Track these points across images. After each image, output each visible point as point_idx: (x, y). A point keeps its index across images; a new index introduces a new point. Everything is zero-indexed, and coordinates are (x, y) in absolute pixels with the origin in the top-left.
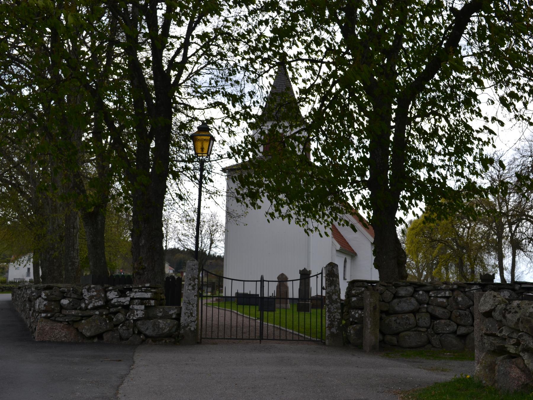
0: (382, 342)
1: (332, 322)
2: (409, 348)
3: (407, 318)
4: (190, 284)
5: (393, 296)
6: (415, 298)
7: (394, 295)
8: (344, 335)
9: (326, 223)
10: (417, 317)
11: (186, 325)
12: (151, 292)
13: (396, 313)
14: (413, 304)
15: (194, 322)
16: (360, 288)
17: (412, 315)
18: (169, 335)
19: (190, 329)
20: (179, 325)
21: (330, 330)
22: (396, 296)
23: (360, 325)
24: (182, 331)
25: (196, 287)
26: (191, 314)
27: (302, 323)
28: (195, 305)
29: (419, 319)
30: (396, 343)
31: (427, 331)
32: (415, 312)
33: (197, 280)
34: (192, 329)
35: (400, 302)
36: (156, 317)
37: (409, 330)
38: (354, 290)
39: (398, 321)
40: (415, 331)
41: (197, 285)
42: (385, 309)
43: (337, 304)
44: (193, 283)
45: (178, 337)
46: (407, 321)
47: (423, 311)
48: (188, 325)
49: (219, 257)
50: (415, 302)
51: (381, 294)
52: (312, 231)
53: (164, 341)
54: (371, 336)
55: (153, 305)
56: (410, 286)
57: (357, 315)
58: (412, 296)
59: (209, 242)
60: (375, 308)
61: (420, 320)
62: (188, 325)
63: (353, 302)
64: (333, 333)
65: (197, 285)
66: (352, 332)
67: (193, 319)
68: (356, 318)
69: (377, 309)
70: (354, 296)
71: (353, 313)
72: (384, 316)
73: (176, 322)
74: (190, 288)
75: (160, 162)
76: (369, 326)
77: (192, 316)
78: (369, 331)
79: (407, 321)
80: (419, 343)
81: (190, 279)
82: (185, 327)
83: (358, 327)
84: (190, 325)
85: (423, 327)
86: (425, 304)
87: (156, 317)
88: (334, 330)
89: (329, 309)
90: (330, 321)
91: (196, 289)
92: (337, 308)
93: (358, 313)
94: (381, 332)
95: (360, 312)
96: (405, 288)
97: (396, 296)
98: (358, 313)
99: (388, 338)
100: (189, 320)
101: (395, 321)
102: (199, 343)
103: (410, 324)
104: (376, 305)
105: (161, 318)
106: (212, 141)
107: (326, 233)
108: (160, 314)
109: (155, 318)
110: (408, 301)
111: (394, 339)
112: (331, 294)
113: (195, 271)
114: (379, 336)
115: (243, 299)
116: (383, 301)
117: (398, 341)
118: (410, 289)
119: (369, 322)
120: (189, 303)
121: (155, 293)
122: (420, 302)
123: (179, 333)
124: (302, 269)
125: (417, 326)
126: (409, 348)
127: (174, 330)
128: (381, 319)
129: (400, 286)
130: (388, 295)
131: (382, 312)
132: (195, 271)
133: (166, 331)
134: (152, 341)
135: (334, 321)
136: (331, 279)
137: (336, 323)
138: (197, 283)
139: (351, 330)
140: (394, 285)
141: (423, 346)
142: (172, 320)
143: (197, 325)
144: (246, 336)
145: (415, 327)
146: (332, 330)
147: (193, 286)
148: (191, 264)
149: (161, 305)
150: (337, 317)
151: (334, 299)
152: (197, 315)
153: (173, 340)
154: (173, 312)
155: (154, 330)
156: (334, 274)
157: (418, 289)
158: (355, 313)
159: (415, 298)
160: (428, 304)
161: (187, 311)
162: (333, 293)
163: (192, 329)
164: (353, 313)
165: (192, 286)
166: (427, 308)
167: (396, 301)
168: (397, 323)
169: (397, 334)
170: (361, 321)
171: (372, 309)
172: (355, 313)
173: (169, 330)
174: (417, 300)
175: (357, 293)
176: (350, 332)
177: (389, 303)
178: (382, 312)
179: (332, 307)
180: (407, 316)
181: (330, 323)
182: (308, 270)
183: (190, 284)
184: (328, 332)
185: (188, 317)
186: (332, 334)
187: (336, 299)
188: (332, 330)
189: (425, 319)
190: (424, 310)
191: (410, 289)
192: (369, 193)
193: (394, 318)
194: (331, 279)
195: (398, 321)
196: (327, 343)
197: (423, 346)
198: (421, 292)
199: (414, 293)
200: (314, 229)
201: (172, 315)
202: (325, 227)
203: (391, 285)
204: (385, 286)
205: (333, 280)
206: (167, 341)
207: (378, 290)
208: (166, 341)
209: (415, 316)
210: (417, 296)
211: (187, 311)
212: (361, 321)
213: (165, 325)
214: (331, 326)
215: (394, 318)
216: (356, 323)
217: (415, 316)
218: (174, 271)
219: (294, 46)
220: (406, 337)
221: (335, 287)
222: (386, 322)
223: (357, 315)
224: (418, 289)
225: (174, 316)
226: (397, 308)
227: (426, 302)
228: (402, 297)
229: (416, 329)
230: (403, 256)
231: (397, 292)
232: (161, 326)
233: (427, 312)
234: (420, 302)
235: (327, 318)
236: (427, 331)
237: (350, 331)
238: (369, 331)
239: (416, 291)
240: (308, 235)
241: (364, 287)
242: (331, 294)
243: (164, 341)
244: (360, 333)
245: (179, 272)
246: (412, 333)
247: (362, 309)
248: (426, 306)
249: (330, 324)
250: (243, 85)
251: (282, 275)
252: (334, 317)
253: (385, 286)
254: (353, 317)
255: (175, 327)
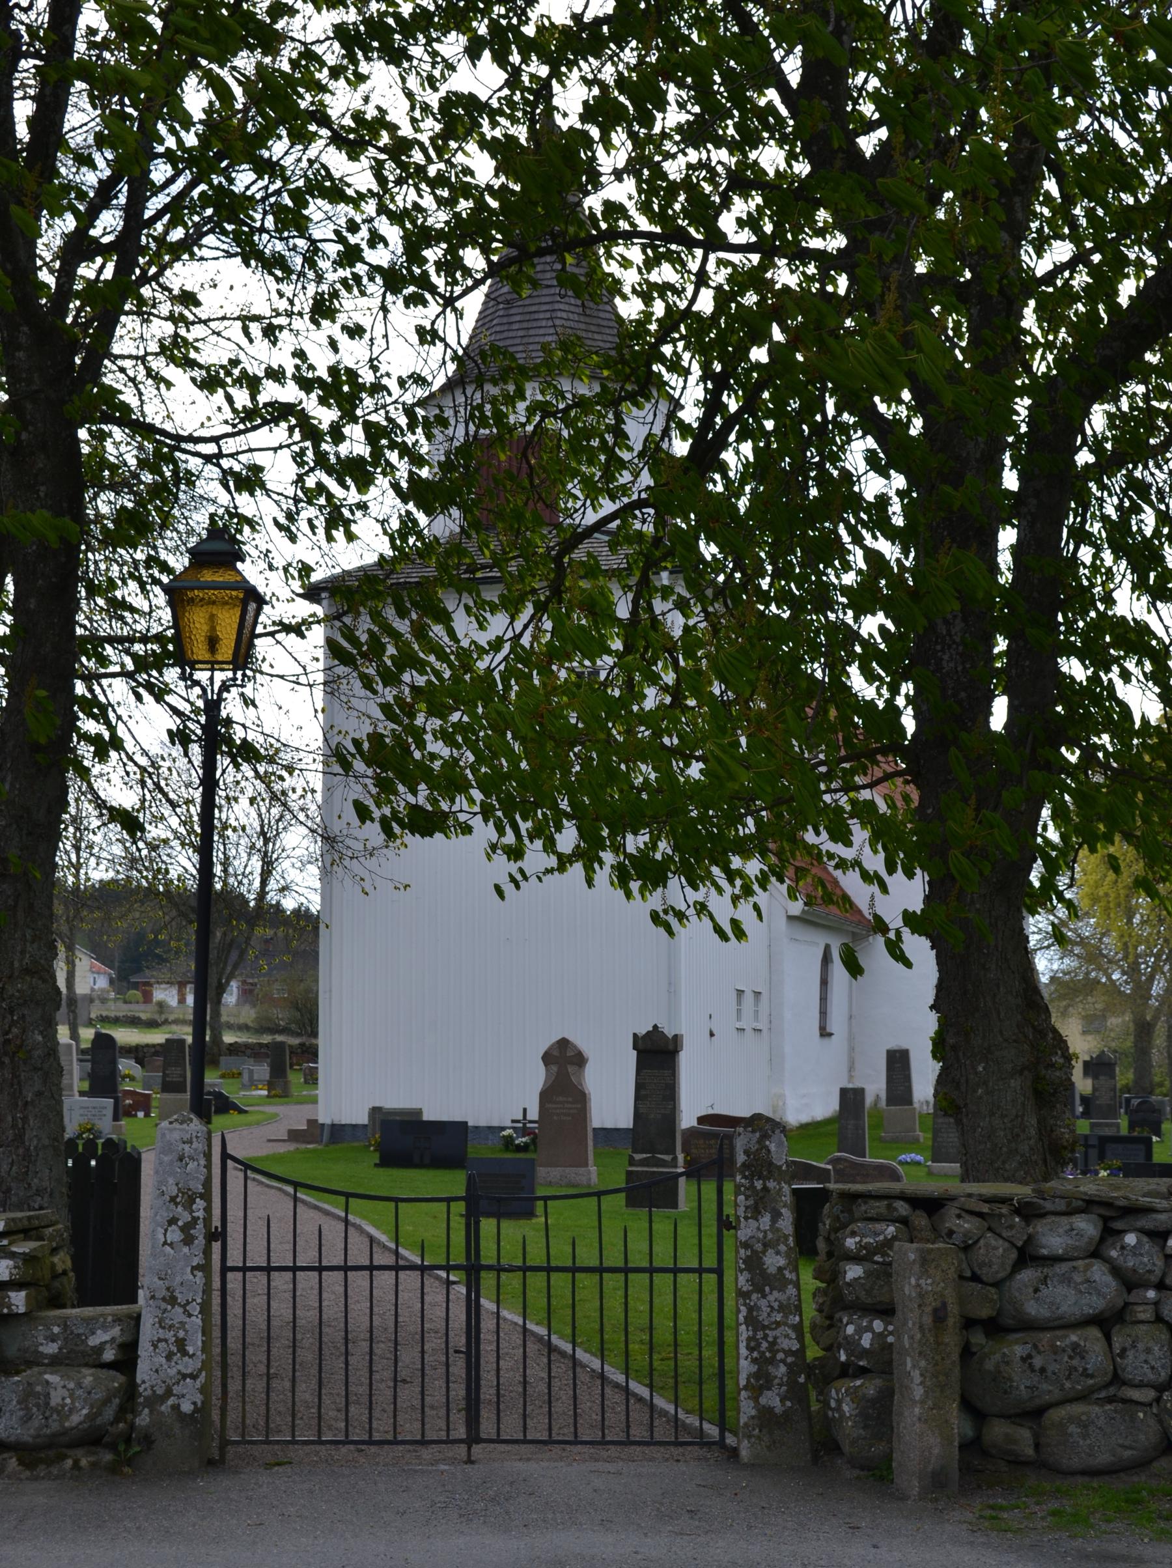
0: (972, 1447)
1: (763, 1363)
2: (1084, 1473)
3: (1075, 1346)
4: (172, 1221)
5: (1014, 1255)
6: (1107, 1260)
7: (1022, 1251)
8: (815, 1407)
9: (738, 882)
10: (1118, 1342)
11: (160, 1392)
12: (12, 1255)
13: (1029, 1326)
14: (1098, 1287)
15: (194, 1377)
16: (878, 1226)
17: (1094, 1332)
18: (92, 1438)
19: (176, 1408)
20: (131, 1390)
21: (756, 1399)
22: (1027, 1256)
23: (878, 1382)
24: (143, 1419)
25: (199, 1231)
26: (181, 1344)
27: (639, 1318)
28: (195, 1309)
29: (1123, 1353)
30: (1030, 1451)
31: (1158, 1400)
32: (1106, 1322)
33: (200, 1204)
34: (186, 1407)
35: (1044, 1280)
36: (33, 1360)
37: (1082, 1397)
38: (853, 1234)
39: (1038, 1362)
40: (1110, 1400)
41: (200, 1225)
42: (985, 1312)
43: (782, 1289)
44: (185, 1217)
45: (128, 1440)
46: (1075, 1362)
47: (1142, 1316)
48: (169, 1393)
49: (301, 914)
50: (1109, 1278)
51: (966, 1248)
52: (681, 916)
53: (69, 1462)
54: (925, 1430)
55: (22, 1310)
56: (1082, 1212)
57: (866, 1341)
58: (1096, 1253)
59: (256, 864)
60: (939, 1316)
61: (1130, 1354)
62: (169, 1393)
63: (849, 1284)
64: (770, 1410)
65: (200, 1225)
66: (846, 1408)
67: (190, 1365)
68: (865, 1353)
69: (951, 1321)
70: (855, 1258)
71: (850, 1330)
72: (978, 1338)
73: (117, 1380)
74: (175, 1235)
75: (42, 693)
76: (918, 1392)
77: (185, 1353)
78: (917, 1410)
79: (1075, 1362)
80: (1127, 1454)
81: (173, 1199)
82: (155, 1400)
83: (870, 1387)
84: (176, 1390)
85: (1141, 1385)
86: (1146, 1286)
87: (33, 1360)
88: (772, 1399)
89: (750, 1309)
90: (754, 1361)
91: (200, 1241)
92: (782, 1308)
93: (869, 1328)
94: (967, 1405)
95: (878, 1325)
96: (1064, 1220)
97: (1027, 1256)
98: (869, 1328)
99: (998, 1430)
100: (172, 1372)
101: (1023, 1359)
102: (214, 1464)
103: (1086, 1374)
104: (944, 1304)
105: (55, 1362)
106: (252, 606)
107: (735, 923)
108: (51, 1349)
109: (30, 1364)
110: (1078, 1278)
111: (1024, 1435)
112: (759, 1247)
113: (192, 1166)
114: (959, 1424)
115: (407, 1141)
116: (975, 1278)
117: (1037, 1446)
118: (1087, 1226)
119: (916, 1374)
120: (172, 1300)
121: (29, 1259)
122: (1129, 1282)
123: (132, 1426)
124: (642, 1030)
125: (1117, 1379)
126: (1084, 1473)
127: (109, 1413)
128: (967, 1352)
129: (1043, 1215)
130: (995, 1253)
131: (969, 1323)
132: (192, 1166)
133: (75, 1419)
134: (21, 1462)
135: (772, 1361)
136: (759, 1185)
137: (783, 1369)
138: (200, 1214)
139: (845, 1401)
140: (1017, 1211)
141: (1140, 1465)
142: (104, 1373)
143: (204, 1390)
144: (410, 1429)
145: (1107, 1386)
146: (763, 1401)
147: (186, 1229)
148: (176, 1135)
149: (56, 1302)
150: (785, 1344)
151: (772, 1270)
152: (205, 1348)
153: (108, 1457)
154: (104, 1337)
155: (27, 1419)
156: (771, 1164)
157: (1118, 1225)
158: (860, 1331)
159: (1107, 1260)
160: (1160, 1286)
161: (162, 1334)
162: (766, 1245)
163: (186, 1407)
164: (850, 1330)
165: (182, 1229)
166: (1156, 1303)
167: (1027, 1275)
168: (1031, 1368)
169: (1034, 1414)
170: (882, 1362)
171: (928, 1320)
172: (860, 1331)
173: (90, 1417)
174: (1116, 1271)
175: (866, 1247)
176: (839, 1409)
177: (997, 1284)
178: (969, 1323)
179: (763, 1303)
180: (1074, 1338)
181: (754, 1368)
182: (669, 1032)
183: (172, 1221)
184: (747, 1409)
185: (169, 1357)
186: (765, 1416)
187: (780, 1269)
188: (763, 1401)
189: (1148, 1351)
190: (1145, 1314)
191: (1087, 1226)
192: (906, 798)
193: (1019, 1350)
194: (759, 1185)
195: (1038, 1362)
196: (744, 1453)
197: (1140, 1465)
198: (1131, 1239)
199: (1102, 1240)
200: (691, 912)
201: (100, 1349)
202: (735, 899)
203: (1005, 1210)
204: (980, 1215)
205: (765, 1189)
206: (84, 1462)
207: (951, 1233)
208: (76, 1463)
209: (1108, 1338)
210: (1114, 1254)
211: (162, 1334)
212: (882, 1362)
213: (71, 1396)
214: (761, 1382)
215: (1019, 1350)
216: (863, 1372)
217: (1108, 1338)
218: (111, 981)
219: (539, 844)
220: (1073, 1429)
221: (774, 1220)
222: (989, 1365)
223: (866, 1341)
224: (1118, 1225)
225: (109, 1355)
226: (1032, 1309)
227: (1154, 1279)
228: (1055, 1259)
229: (1112, 1390)
230: (1058, 1059)
231: (1030, 1239)
232: (55, 1400)
233: (1159, 1319)
234: (1129, 1282)
235: (743, 1351)
236: (1158, 1400)
237: (839, 1402)
238: (917, 1410)
239: (1110, 1233)
240: (670, 933)
241: (893, 1221)
242: (759, 1247)
243: (69, 1462)
244: (880, 1414)
245: (135, 986)
246: (1097, 1409)
247: (887, 1311)
248: (1151, 1294)
249: (757, 1375)
250: (380, 342)
251: (564, 1043)
252: (773, 1343)
253: (980, 1215)
254: (851, 1345)
255: (117, 1401)
